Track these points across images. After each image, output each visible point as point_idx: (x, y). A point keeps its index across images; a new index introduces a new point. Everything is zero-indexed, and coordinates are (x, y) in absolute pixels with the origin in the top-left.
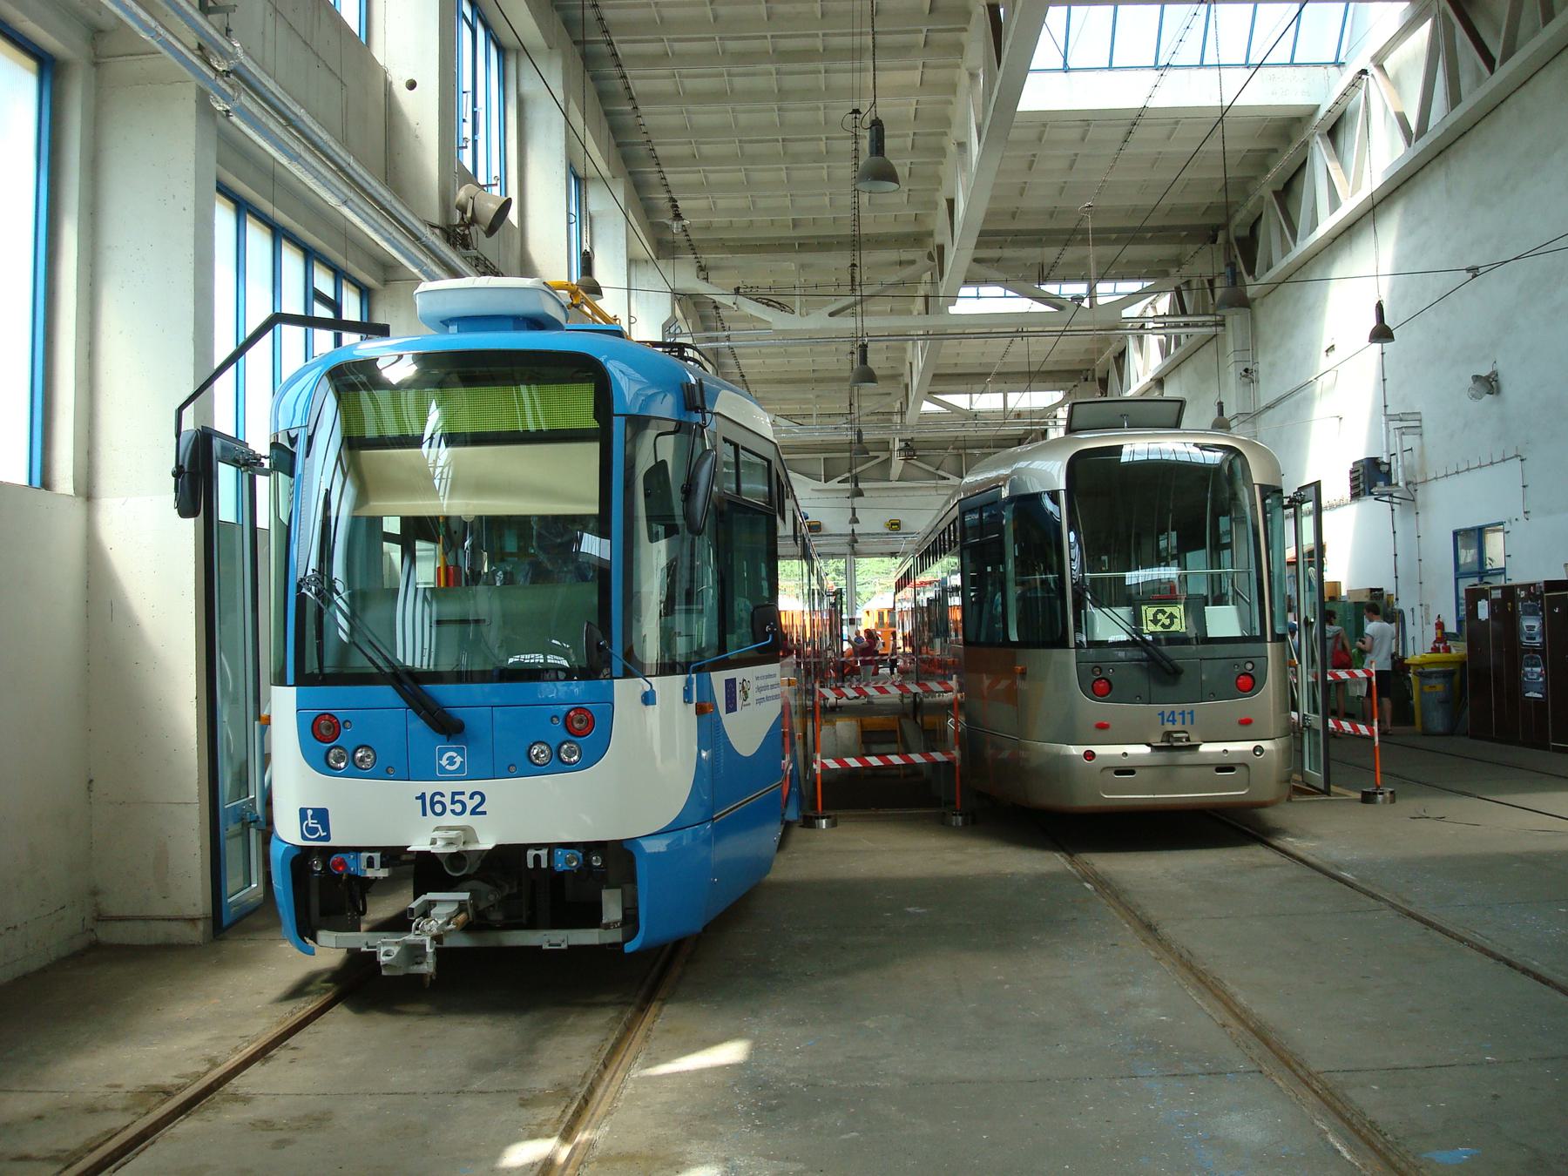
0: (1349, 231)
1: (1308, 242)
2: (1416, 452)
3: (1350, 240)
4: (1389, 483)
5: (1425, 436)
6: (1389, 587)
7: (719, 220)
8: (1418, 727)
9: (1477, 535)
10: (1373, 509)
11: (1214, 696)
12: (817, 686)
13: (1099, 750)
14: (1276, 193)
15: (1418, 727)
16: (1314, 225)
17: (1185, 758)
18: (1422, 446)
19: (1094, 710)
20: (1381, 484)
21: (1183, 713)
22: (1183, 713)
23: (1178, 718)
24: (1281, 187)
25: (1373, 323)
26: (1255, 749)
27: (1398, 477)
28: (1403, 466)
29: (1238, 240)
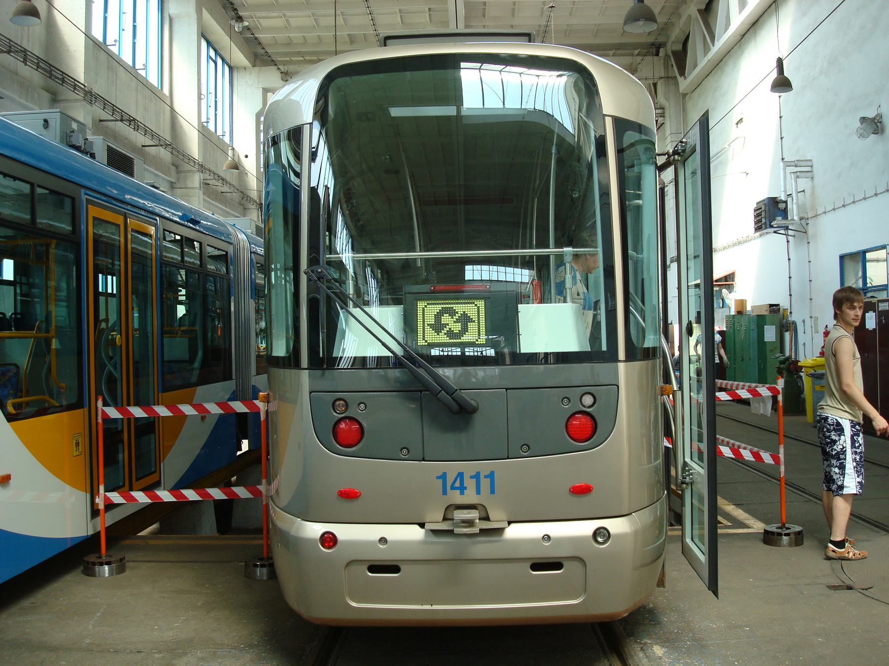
0: (754, 26)
1: (723, 39)
2: (808, 193)
3: (755, 33)
4: (785, 217)
5: (816, 179)
6: (784, 304)
7: (296, 36)
8: (809, 417)
9: (860, 257)
10: (774, 241)
11: (528, 449)
12: (100, 403)
13: (344, 532)
14: (699, 11)
15: (809, 417)
16: (728, 24)
17: (483, 548)
18: (813, 188)
19: (349, 469)
20: (780, 218)
21: (477, 477)
22: (477, 477)
23: (470, 484)
24: (703, 7)
25: (774, 75)
26: (596, 533)
27: (794, 213)
28: (797, 203)
29: (674, 53)
